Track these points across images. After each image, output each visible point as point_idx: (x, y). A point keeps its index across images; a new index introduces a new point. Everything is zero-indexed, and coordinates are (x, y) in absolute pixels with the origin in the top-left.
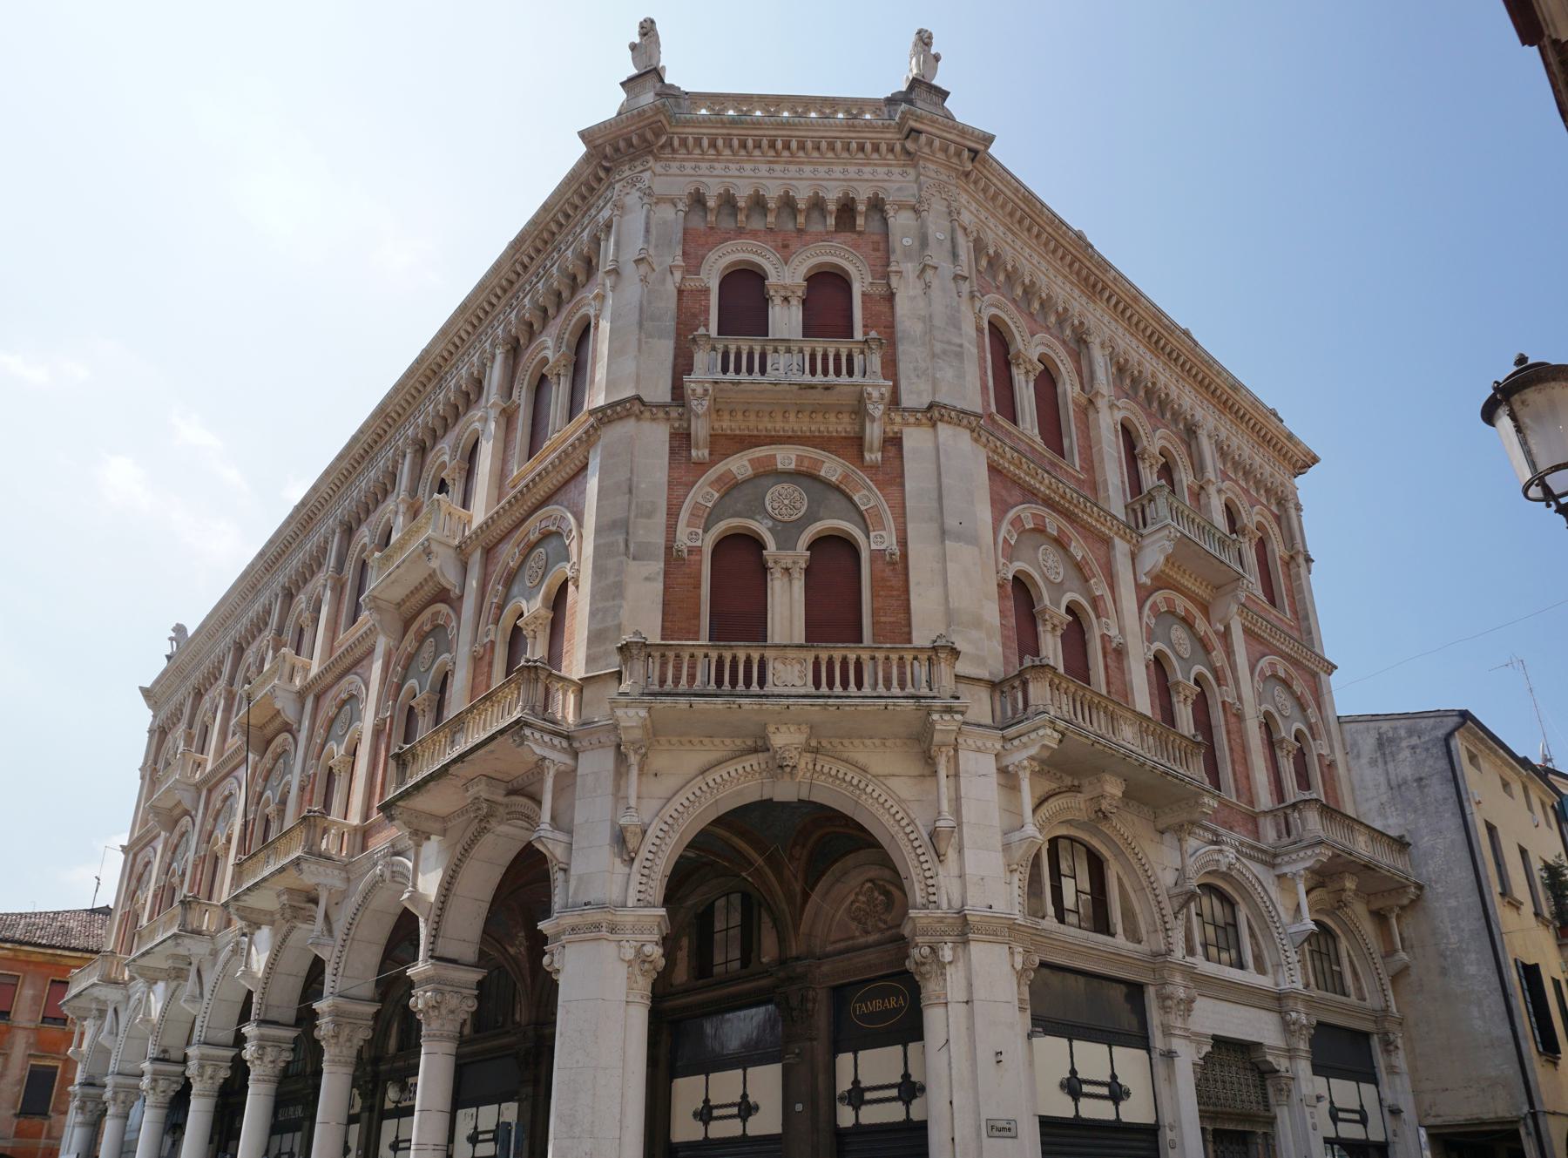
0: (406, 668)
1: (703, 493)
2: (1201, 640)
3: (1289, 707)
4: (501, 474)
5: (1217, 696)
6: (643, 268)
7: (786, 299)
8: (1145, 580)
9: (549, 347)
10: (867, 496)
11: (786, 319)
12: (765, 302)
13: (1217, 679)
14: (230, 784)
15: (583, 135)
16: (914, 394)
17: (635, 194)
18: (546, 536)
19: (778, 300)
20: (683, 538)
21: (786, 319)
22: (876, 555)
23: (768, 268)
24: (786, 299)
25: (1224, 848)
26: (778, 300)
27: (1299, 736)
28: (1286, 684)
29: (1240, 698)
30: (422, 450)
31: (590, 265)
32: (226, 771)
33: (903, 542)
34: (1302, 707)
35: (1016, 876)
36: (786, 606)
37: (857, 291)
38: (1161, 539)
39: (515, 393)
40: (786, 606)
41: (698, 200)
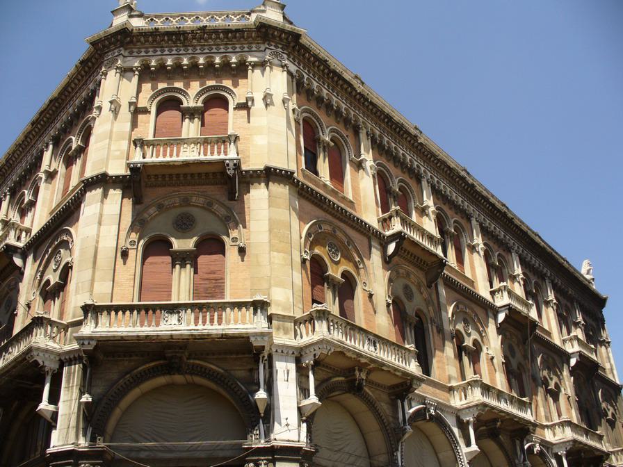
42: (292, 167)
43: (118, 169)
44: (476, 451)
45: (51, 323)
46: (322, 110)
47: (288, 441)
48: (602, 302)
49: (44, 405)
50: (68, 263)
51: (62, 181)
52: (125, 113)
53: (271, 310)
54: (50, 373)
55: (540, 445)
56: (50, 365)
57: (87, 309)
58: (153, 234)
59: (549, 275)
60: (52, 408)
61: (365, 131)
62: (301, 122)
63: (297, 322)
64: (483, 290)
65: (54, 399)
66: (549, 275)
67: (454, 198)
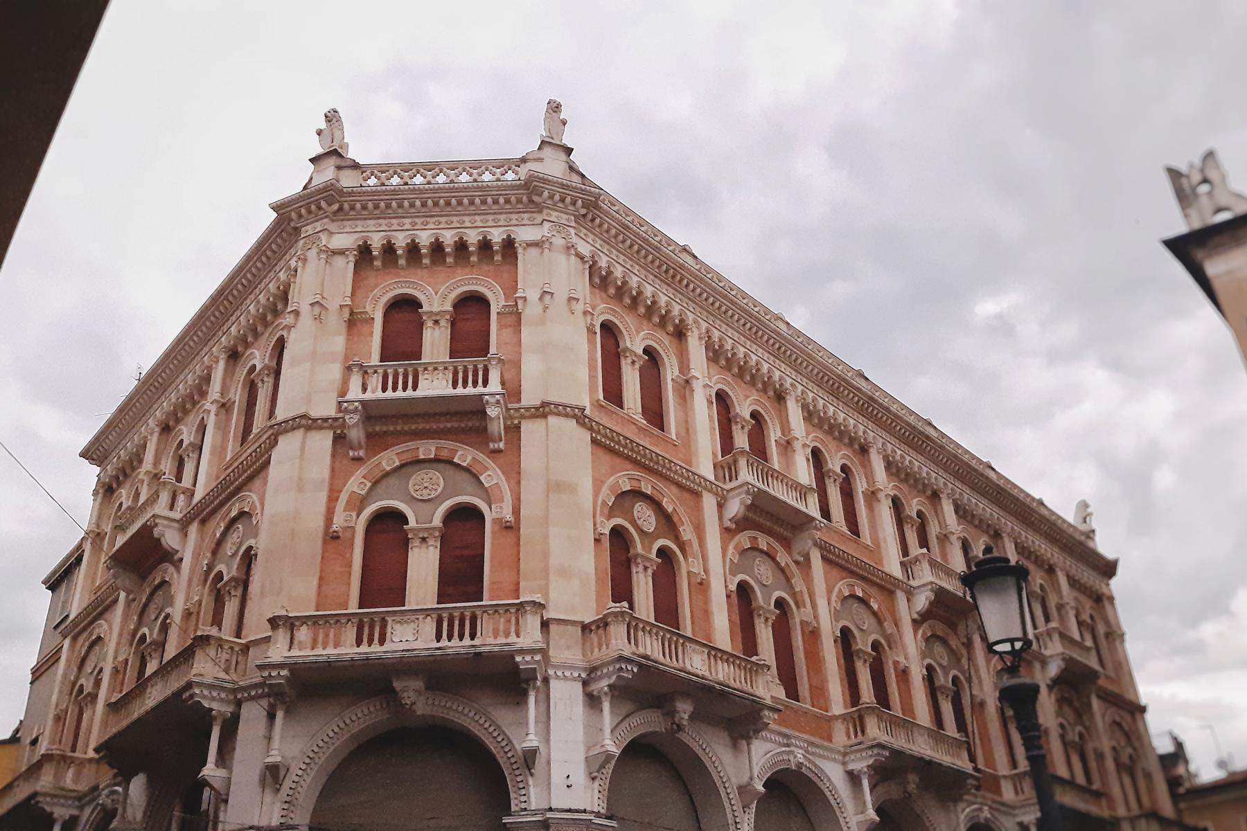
0: (215, 552)
1: (356, 484)
2: (782, 570)
3: (868, 622)
4: (219, 451)
5: (798, 616)
6: (317, 310)
7: (436, 322)
8: (728, 524)
9: (258, 357)
10: (492, 476)
11: (435, 342)
12: (420, 325)
13: (797, 603)
14: (102, 627)
15: (275, 208)
16: (530, 398)
17: (314, 251)
18: (242, 514)
19: (430, 324)
20: (339, 521)
21: (435, 342)
22: (498, 521)
23: (421, 297)
24: (436, 322)
25: (792, 748)
26: (430, 324)
27: (876, 646)
28: (863, 601)
29: (816, 617)
30: (234, 356)
31: (284, 296)
32: (99, 609)
33: (516, 512)
34: (880, 622)
35: (596, 783)
36: (423, 567)
37: (494, 310)
38: (740, 494)
39: (163, 462)
40: (423, 567)
41: (364, 251)
42: (585, 402)
43: (325, 408)
44: (873, 822)
45: (220, 643)
46: (1163, 746)
47: (570, 811)
48: (1108, 569)
49: (210, 770)
50: (250, 548)
51: (17, 790)
52: (336, 321)
53: (550, 614)
54: (219, 721)
55: (991, 808)
56: (219, 707)
57: (274, 622)
58: (409, 291)
59: (1061, 564)
60: (222, 773)
61: (696, 332)
62: (598, 330)
63: (585, 628)
64: (892, 565)
65: (224, 758)
66: (1061, 564)
67: (841, 420)
